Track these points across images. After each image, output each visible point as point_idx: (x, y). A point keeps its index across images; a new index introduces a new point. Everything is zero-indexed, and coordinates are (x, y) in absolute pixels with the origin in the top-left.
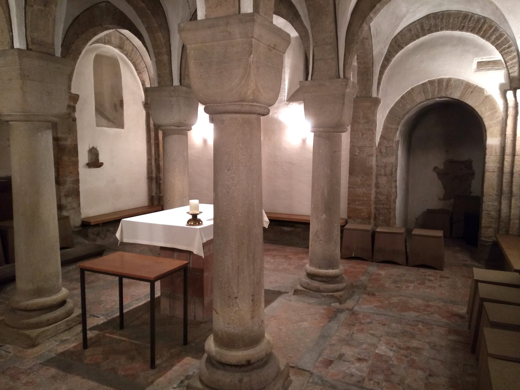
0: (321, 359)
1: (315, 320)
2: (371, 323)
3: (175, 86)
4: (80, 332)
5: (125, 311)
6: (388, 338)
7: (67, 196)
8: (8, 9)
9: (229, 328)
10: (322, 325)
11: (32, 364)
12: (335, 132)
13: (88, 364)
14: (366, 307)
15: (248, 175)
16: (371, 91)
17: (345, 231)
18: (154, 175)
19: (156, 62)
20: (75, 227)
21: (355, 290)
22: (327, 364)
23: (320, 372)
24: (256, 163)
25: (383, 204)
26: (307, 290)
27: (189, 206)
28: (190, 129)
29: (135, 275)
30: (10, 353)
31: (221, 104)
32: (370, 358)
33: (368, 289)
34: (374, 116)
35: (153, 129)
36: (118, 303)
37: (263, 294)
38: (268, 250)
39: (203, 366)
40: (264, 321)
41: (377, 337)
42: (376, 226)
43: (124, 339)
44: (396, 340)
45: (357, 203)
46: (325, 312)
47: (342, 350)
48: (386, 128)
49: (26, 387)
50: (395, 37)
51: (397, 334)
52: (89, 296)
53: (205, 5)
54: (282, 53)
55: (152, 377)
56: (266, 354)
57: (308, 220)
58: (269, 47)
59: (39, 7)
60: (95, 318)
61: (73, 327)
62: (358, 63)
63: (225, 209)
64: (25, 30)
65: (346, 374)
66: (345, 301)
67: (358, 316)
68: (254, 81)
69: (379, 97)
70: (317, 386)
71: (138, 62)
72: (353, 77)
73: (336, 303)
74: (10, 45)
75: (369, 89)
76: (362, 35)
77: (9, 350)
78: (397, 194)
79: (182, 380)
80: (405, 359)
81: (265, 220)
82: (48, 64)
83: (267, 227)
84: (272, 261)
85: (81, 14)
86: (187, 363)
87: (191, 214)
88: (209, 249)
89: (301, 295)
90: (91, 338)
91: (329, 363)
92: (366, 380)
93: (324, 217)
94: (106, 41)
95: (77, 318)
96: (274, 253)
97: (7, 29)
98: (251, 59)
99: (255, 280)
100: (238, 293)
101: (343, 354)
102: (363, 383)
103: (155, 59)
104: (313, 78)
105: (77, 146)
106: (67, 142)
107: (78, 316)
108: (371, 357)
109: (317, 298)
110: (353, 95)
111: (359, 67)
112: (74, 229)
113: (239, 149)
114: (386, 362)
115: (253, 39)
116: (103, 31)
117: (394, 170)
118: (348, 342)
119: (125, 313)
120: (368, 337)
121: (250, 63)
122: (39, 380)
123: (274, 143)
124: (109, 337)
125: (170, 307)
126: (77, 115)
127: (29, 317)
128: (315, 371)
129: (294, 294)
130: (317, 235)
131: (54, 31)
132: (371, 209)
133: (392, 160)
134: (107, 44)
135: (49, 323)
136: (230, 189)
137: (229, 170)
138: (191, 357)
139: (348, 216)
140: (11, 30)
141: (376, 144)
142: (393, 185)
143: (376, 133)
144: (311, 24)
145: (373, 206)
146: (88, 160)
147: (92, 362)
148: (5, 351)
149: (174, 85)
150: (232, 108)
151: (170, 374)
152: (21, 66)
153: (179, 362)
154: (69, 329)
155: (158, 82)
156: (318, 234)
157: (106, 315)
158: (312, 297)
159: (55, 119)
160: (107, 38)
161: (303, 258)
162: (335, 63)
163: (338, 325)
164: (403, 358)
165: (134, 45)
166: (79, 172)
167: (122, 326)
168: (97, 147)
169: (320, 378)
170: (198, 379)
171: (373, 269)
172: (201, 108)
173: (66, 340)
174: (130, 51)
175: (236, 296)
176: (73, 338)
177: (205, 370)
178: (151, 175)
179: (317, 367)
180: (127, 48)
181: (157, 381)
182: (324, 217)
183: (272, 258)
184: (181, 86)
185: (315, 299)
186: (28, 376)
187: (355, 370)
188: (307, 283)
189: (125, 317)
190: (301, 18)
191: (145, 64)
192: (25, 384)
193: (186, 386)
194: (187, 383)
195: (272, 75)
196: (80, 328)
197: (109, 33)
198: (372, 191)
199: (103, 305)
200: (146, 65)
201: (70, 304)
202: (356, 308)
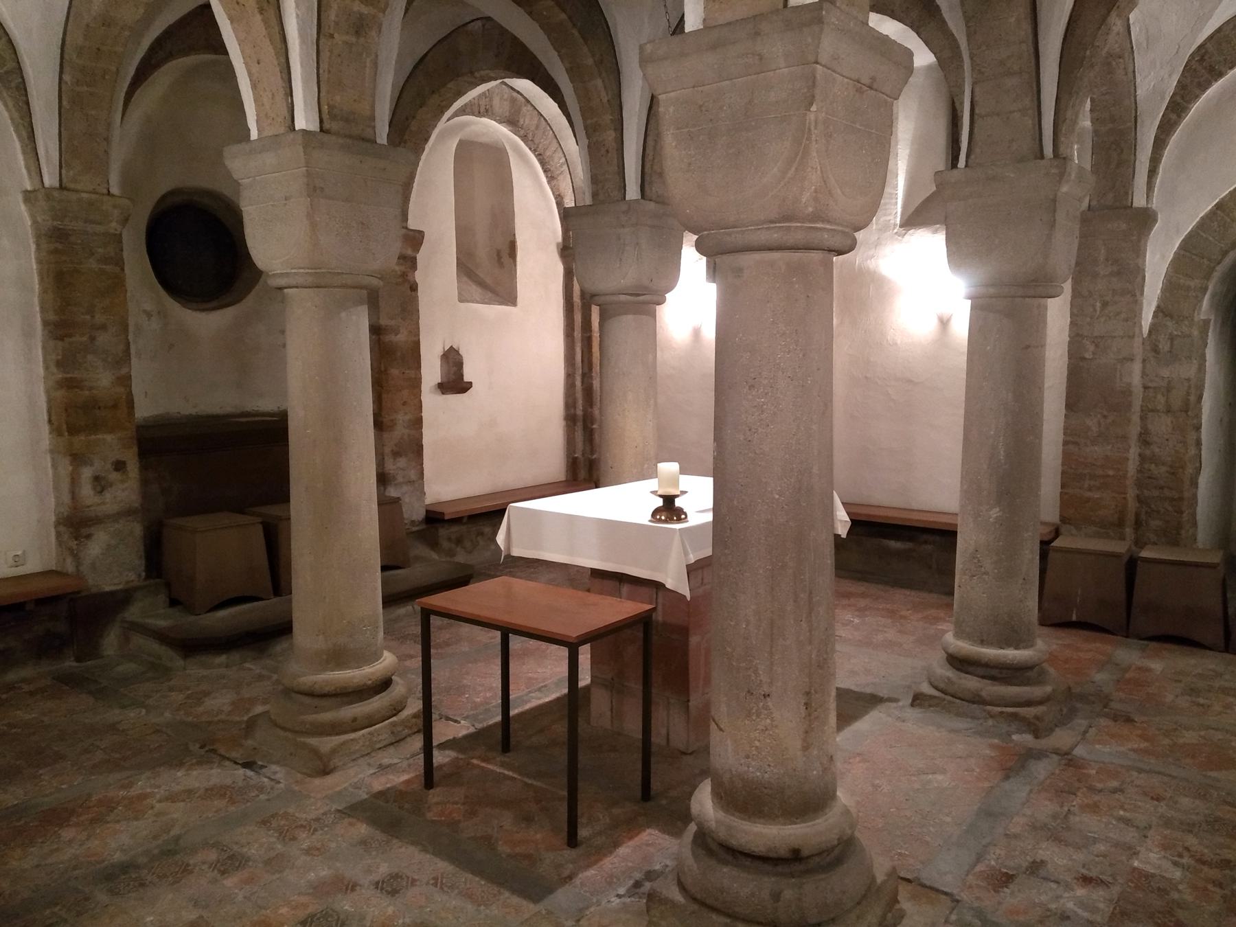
0: (979, 868)
1: (967, 770)
2: (1122, 791)
4: (419, 750)
5: (513, 712)
6: (1167, 832)
7: (396, 454)
8: (283, 46)
9: (748, 767)
10: (987, 785)
12: (1029, 297)
13: (433, 822)
14: (1107, 749)
15: (799, 399)
17: (1052, 555)
18: (579, 412)
19: (589, 147)
23: (978, 898)
24: (818, 369)
25: (1162, 488)
27: (657, 479)
30: (279, 782)
31: (736, 229)
33: (1113, 705)
34: (1138, 257)
35: (580, 304)
38: (847, 595)
39: (687, 852)
40: (834, 757)
41: (1138, 827)
42: (1139, 543)
43: (510, 773)
44: (1191, 841)
46: (993, 754)
48: (1171, 287)
49: (308, 859)
50: (1199, 47)
51: (1194, 825)
54: (890, 97)
56: (839, 839)
57: (950, 524)
59: (346, 38)
61: (406, 737)
63: (740, 480)
64: (317, 90)
65: (1049, 913)
68: (819, 168)
69: (1154, 206)
71: (548, 153)
72: (1079, 154)
74: (287, 125)
75: (1124, 187)
76: (1106, 44)
77: (278, 776)
78: (1200, 461)
79: (637, 879)
80: (1218, 890)
81: (839, 518)
83: (844, 536)
84: (856, 621)
85: (431, 50)
87: (661, 496)
88: (702, 579)
90: (441, 767)
91: (1003, 880)
93: (997, 513)
95: (414, 720)
96: (862, 603)
97: (282, 90)
98: (812, 117)
100: (771, 684)
101: (1042, 862)
104: (970, 161)
106: (398, 336)
107: (415, 716)
108: (1118, 878)
109: (973, 718)
110: (1079, 201)
111: (1096, 132)
112: (410, 527)
114: (1162, 892)
117: (1192, 398)
118: (1056, 833)
119: (513, 717)
120: (1111, 826)
121: (809, 123)
122: (333, 845)
123: (865, 331)
124: (478, 766)
126: (419, 276)
127: (317, 709)
128: (965, 896)
129: (912, 705)
131: (375, 88)
132: (1125, 498)
133: (1187, 370)
134: (484, 116)
135: (355, 725)
136: (755, 433)
137: (752, 387)
138: (660, 831)
140: (290, 93)
141: (1144, 330)
142: (1192, 436)
143: (1144, 301)
144: (968, 27)
145: (1131, 493)
147: (443, 818)
148: (269, 778)
150: (763, 237)
152: (308, 167)
153: (631, 838)
156: (979, 556)
157: (472, 718)
158: (958, 715)
159: (375, 282)
160: (483, 103)
161: (937, 620)
162: (1030, 122)
163: (1028, 788)
164: (1210, 887)
165: (541, 115)
167: (506, 747)
170: (675, 882)
171: (1128, 655)
172: (689, 241)
174: (533, 128)
176: (405, 763)
177: (690, 861)
178: (572, 411)
180: (527, 122)
181: (580, 876)
182: (997, 513)
183: (856, 613)
184: (643, 200)
185: (969, 720)
186: (312, 834)
188: (946, 680)
189: (514, 726)
190: (942, 14)
191: (565, 156)
192: (308, 852)
193: (646, 895)
194: (649, 888)
196: (417, 743)
198: (1128, 451)
199: (467, 696)
200: (566, 159)
201: (398, 689)
202: (1079, 751)
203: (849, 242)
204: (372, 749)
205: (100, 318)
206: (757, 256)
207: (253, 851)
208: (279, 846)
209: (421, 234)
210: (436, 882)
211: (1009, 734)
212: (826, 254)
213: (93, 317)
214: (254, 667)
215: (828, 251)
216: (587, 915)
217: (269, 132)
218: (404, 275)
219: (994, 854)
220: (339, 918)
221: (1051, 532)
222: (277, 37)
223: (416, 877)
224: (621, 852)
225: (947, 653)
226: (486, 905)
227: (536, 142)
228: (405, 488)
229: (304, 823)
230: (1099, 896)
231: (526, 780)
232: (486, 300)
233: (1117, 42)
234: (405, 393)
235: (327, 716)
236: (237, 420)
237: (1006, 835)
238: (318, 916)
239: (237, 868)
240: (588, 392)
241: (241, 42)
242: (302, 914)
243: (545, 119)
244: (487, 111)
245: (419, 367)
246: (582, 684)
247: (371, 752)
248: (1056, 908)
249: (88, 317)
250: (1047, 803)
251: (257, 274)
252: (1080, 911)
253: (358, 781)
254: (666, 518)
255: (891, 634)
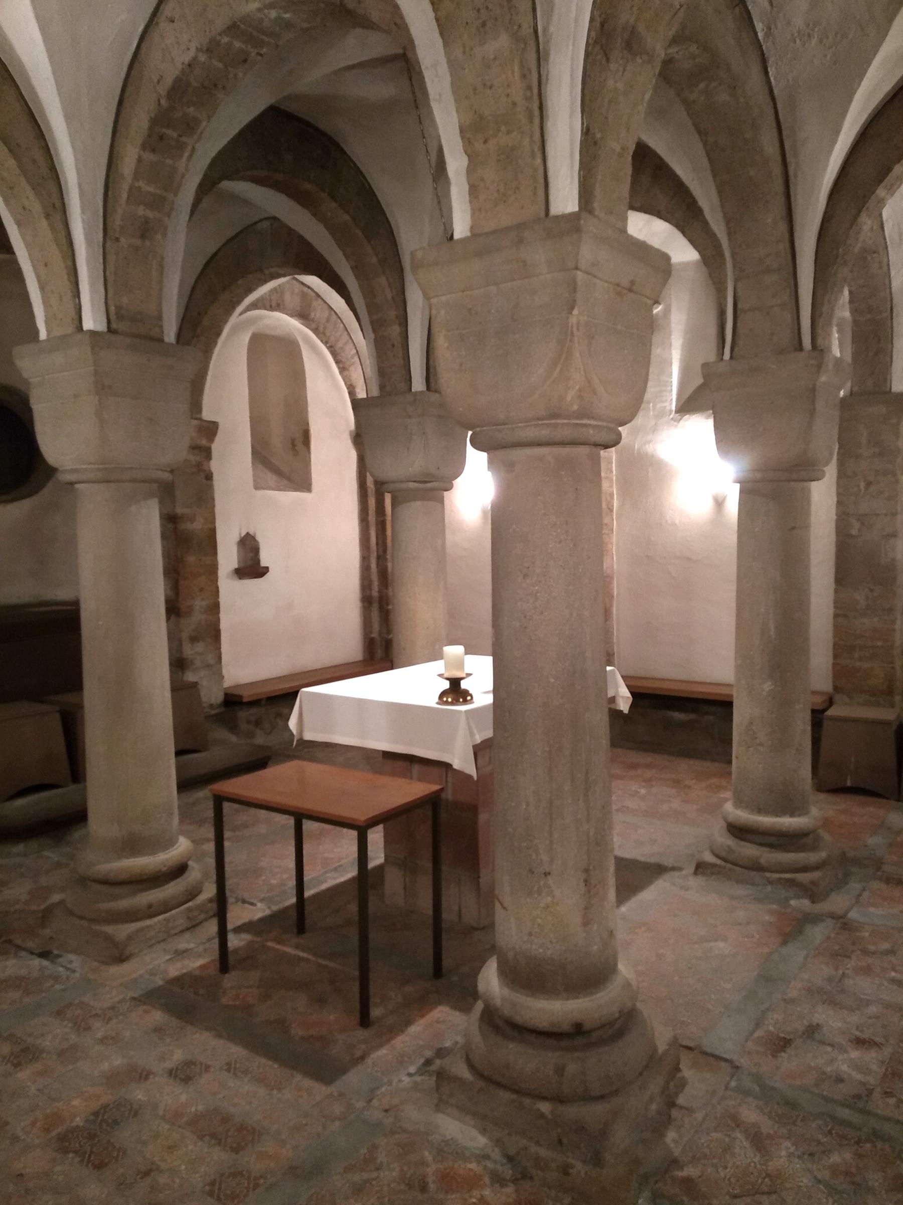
0: (758, 1033)
3: (416, 392)
5: (308, 894)
7: (193, 639)
9: (532, 944)
10: (766, 950)
11: (117, 999)
14: (880, 911)
16: (888, 377)
17: (826, 724)
18: (375, 593)
19: (376, 341)
20: (211, 706)
21: (853, 869)
22: (774, 1047)
23: (756, 1064)
24: (589, 558)
26: (729, 865)
28: (449, 488)
29: (321, 813)
30: (74, 971)
32: (887, 1041)
33: (886, 868)
36: (294, 872)
37: (612, 868)
39: (475, 1029)
45: (857, 654)
47: (816, 1015)
52: (234, 857)
53: (469, 204)
55: (363, 1047)
56: (620, 1012)
58: (619, 289)
60: (246, 905)
62: (854, 311)
65: (824, 1077)
66: (827, 895)
67: (858, 934)
68: (582, 369)
70: (750, 1099)
71: (340, 345)
73: (801, 900)
79: (428, 1057)
82: (149, 360)
84: (643, 791)
86: (441, 1019)
87: (447, 679)
89: (713, 877)
90: (236, 951)
92: (877, 1094)
94: (274, 304)
96: (649, 773)
98: (573, 320)
99: (591, 834)
101: (818, 1025)
102: (867, 1101)
103: (372, 336)
105: (215, 533)
106: (195, 524)
107: (210, 900)
109: (753, 884)
111: (855, 322)
113: (549, 526)
115: (579, 273)
116: (266, 282)
119: (309, 898)
121: (572, 327)
124: (273, 948)
125: (405, 889)
126: (214, 465)
127: (116, 898)
128: (744, 1062)
129: (696, 873)
130: (751, 733)
131: (161, 290)
132: (893, 668)
134: (276, 310)
135: (152, 911)
136: (530, 620)
137: (526, 576)
139: (833, 685)
140: (77, 294)
146: (239, 562)
149: (413, 390)
150: (531, 433)
151: (403, 1043)
153: (422, 1016)
154: (192, 927)
155: (380, 385)
159: (166, 476)
161: (720, 788)
163: (805, 953)
165: (332, 309)
166: (218, 588)
168: (255, 535)
169: (758, 1078)
170: (464, 1060)
173: (185, 951)
174: (324, 320)
175: (547, 870)
176: (201, 948)
177: (477, 1038)
178: (368, 593)
179: (749, 1053)
182: (768, 687)
183: (643, 784)
184: (428, 392)
186: (107, 1023)
187: (848, 1066)
189: (308, 908)
191: (356, 348)
192: (102, 1041)
195: (626, 351)
196: (212, 927)
197: (279, 285)
199: (263, 878)
200: (357, 351)
201: (194, 874)
202: (853, 915)
203: (613, 437)
204: (169, 934)
206: (528, 451)
207: (47, 1043)
208: (73, 1037)
209: (215, 425)
210: (229, 1067)
211: (787, 900)
212: (594, 449)
214: (52, 855)
215: (594, 445)
216: (378, 1096)
217: (58, 332)
218: (199, 465)
219: (772, 1019)
220: (132, 1107)
221: (824, 701)
222: (64, 241)
223: (210, 1063)
224: (413, 1030)
225: (726, 821)
226: (280, 1090)
227: (328, 334)
228: (203, 673)
229: (99, 1012)
230: (871, 1057)
231: (320, 961)
232: (282, 487)
233: (871, 239)
234: (203, 579)
235: (124, 904)
236: (36, 610)
237: (784, 1000)
238: (111, 1106)
239: (31, 1061)
240: (384, 575)
241: (28, 246)
242: (95, 1105)
243: (334, 311)
244: (278, 305)
245: (215, 553)
246: (371, 865)
248: (831, 1071)
250: (823, 966)
251: (51, 471)
252: (854, 1074)
253: (154, 968)
254: (453, 700)
255: (676, 804)
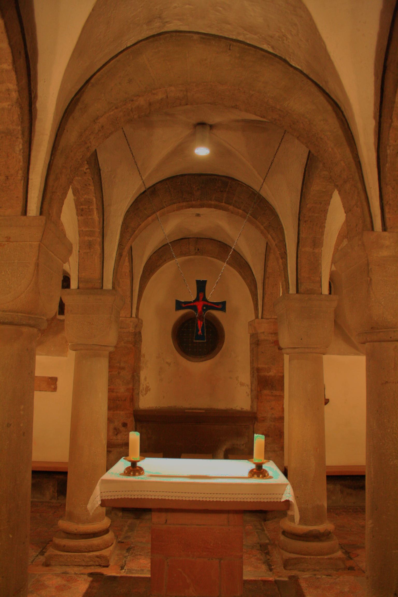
205: (122, 365)
213: (120, 364)
247: (70, 565)
249: (118, 364)
